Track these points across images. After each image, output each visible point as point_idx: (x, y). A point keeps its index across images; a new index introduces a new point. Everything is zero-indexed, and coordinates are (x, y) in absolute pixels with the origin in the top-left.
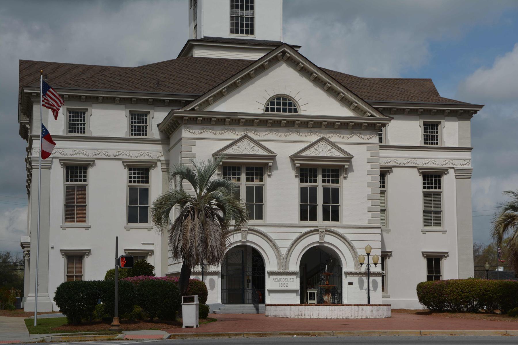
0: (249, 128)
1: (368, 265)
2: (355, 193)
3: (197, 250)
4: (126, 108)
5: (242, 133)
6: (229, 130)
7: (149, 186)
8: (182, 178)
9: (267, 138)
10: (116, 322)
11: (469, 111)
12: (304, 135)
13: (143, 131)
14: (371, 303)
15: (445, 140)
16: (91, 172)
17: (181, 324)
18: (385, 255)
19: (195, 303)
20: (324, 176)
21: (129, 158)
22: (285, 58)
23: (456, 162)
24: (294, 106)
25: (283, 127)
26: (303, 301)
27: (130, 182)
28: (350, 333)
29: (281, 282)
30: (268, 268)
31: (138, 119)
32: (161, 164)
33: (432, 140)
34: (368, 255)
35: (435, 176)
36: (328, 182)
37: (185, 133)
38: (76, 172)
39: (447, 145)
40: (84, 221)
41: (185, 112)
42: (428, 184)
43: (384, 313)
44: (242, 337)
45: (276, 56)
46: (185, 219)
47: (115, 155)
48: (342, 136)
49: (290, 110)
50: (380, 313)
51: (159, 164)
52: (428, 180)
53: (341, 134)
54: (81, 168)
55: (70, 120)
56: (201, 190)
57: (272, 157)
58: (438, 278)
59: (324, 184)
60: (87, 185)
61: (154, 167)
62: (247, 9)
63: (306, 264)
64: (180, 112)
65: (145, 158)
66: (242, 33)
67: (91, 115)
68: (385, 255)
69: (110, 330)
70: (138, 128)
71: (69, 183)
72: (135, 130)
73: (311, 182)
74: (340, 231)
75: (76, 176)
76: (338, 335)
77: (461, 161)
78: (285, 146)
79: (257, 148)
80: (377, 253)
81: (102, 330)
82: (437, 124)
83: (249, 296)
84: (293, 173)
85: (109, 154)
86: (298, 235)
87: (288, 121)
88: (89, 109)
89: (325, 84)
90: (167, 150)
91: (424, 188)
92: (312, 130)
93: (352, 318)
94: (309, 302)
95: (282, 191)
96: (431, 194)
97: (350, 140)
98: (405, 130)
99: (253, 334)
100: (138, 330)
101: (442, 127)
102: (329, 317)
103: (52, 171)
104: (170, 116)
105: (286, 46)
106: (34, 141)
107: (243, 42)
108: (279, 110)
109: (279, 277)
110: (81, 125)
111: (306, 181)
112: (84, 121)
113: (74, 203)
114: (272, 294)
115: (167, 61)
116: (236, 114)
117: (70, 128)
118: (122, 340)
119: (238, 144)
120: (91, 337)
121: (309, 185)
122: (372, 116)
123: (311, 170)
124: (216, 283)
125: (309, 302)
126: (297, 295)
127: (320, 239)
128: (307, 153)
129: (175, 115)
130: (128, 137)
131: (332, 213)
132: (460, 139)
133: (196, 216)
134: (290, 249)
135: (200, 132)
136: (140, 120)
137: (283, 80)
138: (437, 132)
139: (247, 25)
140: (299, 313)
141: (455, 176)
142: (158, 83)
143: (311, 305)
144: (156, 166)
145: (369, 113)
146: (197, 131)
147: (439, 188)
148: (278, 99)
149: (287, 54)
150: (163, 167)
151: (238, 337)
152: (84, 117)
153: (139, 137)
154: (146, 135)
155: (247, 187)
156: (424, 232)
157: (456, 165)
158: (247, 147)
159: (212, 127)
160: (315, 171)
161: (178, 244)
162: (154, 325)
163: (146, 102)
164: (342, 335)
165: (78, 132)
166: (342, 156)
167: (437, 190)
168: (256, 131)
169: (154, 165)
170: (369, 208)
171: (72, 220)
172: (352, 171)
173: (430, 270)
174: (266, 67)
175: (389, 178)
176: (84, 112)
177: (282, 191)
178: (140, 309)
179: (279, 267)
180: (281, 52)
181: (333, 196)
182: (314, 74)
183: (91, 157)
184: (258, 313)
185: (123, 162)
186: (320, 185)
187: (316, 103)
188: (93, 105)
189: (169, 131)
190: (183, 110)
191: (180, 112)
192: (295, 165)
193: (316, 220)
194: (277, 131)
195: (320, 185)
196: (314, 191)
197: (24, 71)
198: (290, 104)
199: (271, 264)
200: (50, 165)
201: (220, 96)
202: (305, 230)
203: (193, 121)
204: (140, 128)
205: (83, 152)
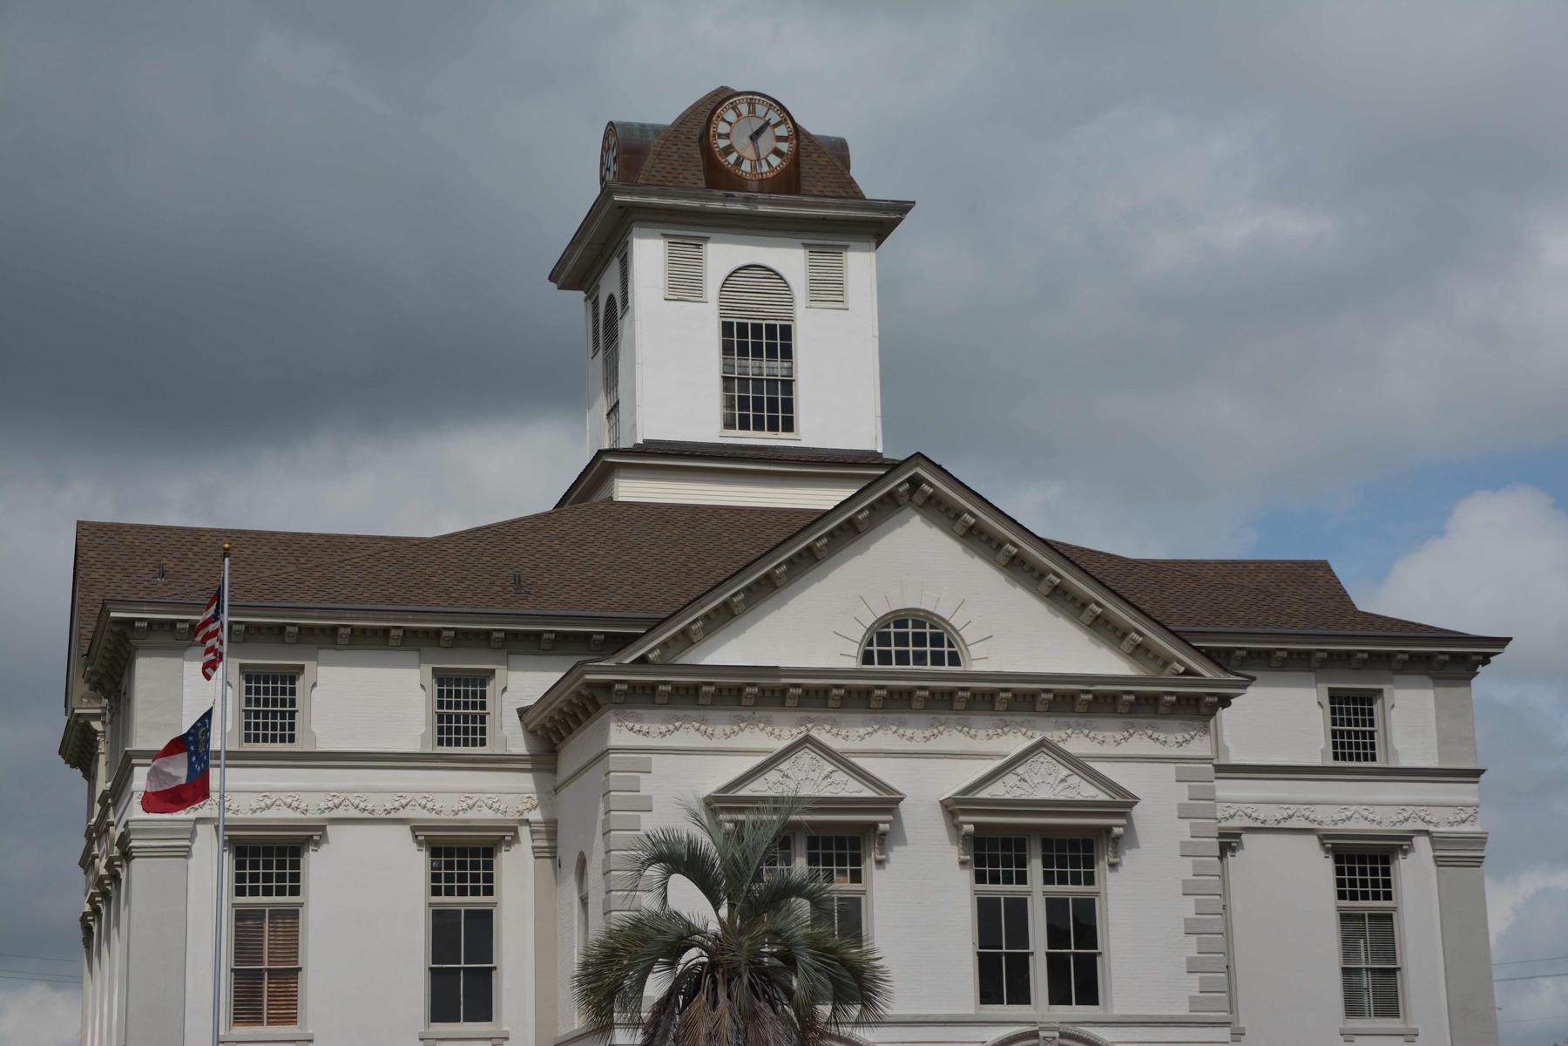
0: (813, 715)
2: (1141, 910)
4: (422, 661)
5: (794, 731)
6: (753, 722)
7: (495, 904)
8: (670, 873)
9: (868, 744)
11: (1465, 656)
12: (982, 733)
13: (474, 732)
15: (1397, 746)
16: (314, 864)
20: (1047, 862)
21: (433, 816)
22: (918, 499)
23: (1435, 815)
24: (950, 645)
25: (918, 711)
31: (458, 694)
32: (532, 832)
33: (457, 732)
35: (1373, 860)
36: (1063, 881)
37: (620, 733)
38: (268, 865)
39: (1405, 762)
40: (291, 1019)
41: (620, 668)
42: (1353, 883)
45: (890, 494)
46: (687, 1003)
47: (388, 806)
48: (1100, 736)
49: (938, 659)
51: (524, 832)
52: (1352, 871)
53: (1097, 728)
54: (281, 851)
55: (248, 701)
57: (889, 803)
59: (1050, 888)
60: (301, 905)
61: (510, 844)
62: (772, 354)
64: (603, 671)
65: (483, 815)
66: (759, 426)
67: (315, 685)
70: (459, 721)
72: (449, 729)
73: (1008, 881)
75: (267, 878)
77: (1439, 807)
78: (928, 771)
79: (841, 776)
85: (370, 807)
87: (933, 693)
88: (500, 671)
91: (1341, 896)
92: (1008, 719)
98: (1280, 717)
101: (1388, 706)
103: (191, 862)
104: (570, 679)
106: (136, 769)
107: (762, 454)
108: (902, 658)
110: (283, 717)
112: (293, 703)
113: (262, 963)
115: (537, 517)
116: (774, 671)
117: (247, 726)
119: (784, 766)
122: (1188, 672)
123: (1006, 844)
128: (996, 791)
129: (588, 677)
130: (429, 750)
131: (1078, 979)
132: (1443, 741)
133: (722, 994)
135: (663, 728)
137: (911, 565)
138: (1372, 724)
139: (773, 404)
141: (1435, 857)
142: (518, 581)
144: (515, 839)
145: (1181, 663)
146: (656, 728)
147: (1388, 896)
148: (901, 623)
150: (537, 844)
152: (293, 692)
153: (461, 750)
154: (483, 743)
155: (1048, 900)
157: (1437, 825)
158: (811, 775)
159: (701, 713)
160: (1021, 845)
163: (482, 639)
165: (274, 740)
168: (835, 723)
169: (508, 836)
171: (256, 1020)
172: (1134, 844)
176: (293, 674)
180: (908, 480)
181: (1077, 931)
182: (1009, 547)
183: (313, 815)
185: (414, 829)
188: (323, 654)
189: (556, 731)
190: (611, 663)
191: (603, 671)
192: (958, 827)
193: (1027, 1001)
194: (902, 724)
195: (1036, 891)
196: (1018, 908)
197: (92, 554)
198: (937, 640)
200: (187, 843)
201: (725, 616)
203: (643, 697)
204: (466, 721)
205: (289, 801)
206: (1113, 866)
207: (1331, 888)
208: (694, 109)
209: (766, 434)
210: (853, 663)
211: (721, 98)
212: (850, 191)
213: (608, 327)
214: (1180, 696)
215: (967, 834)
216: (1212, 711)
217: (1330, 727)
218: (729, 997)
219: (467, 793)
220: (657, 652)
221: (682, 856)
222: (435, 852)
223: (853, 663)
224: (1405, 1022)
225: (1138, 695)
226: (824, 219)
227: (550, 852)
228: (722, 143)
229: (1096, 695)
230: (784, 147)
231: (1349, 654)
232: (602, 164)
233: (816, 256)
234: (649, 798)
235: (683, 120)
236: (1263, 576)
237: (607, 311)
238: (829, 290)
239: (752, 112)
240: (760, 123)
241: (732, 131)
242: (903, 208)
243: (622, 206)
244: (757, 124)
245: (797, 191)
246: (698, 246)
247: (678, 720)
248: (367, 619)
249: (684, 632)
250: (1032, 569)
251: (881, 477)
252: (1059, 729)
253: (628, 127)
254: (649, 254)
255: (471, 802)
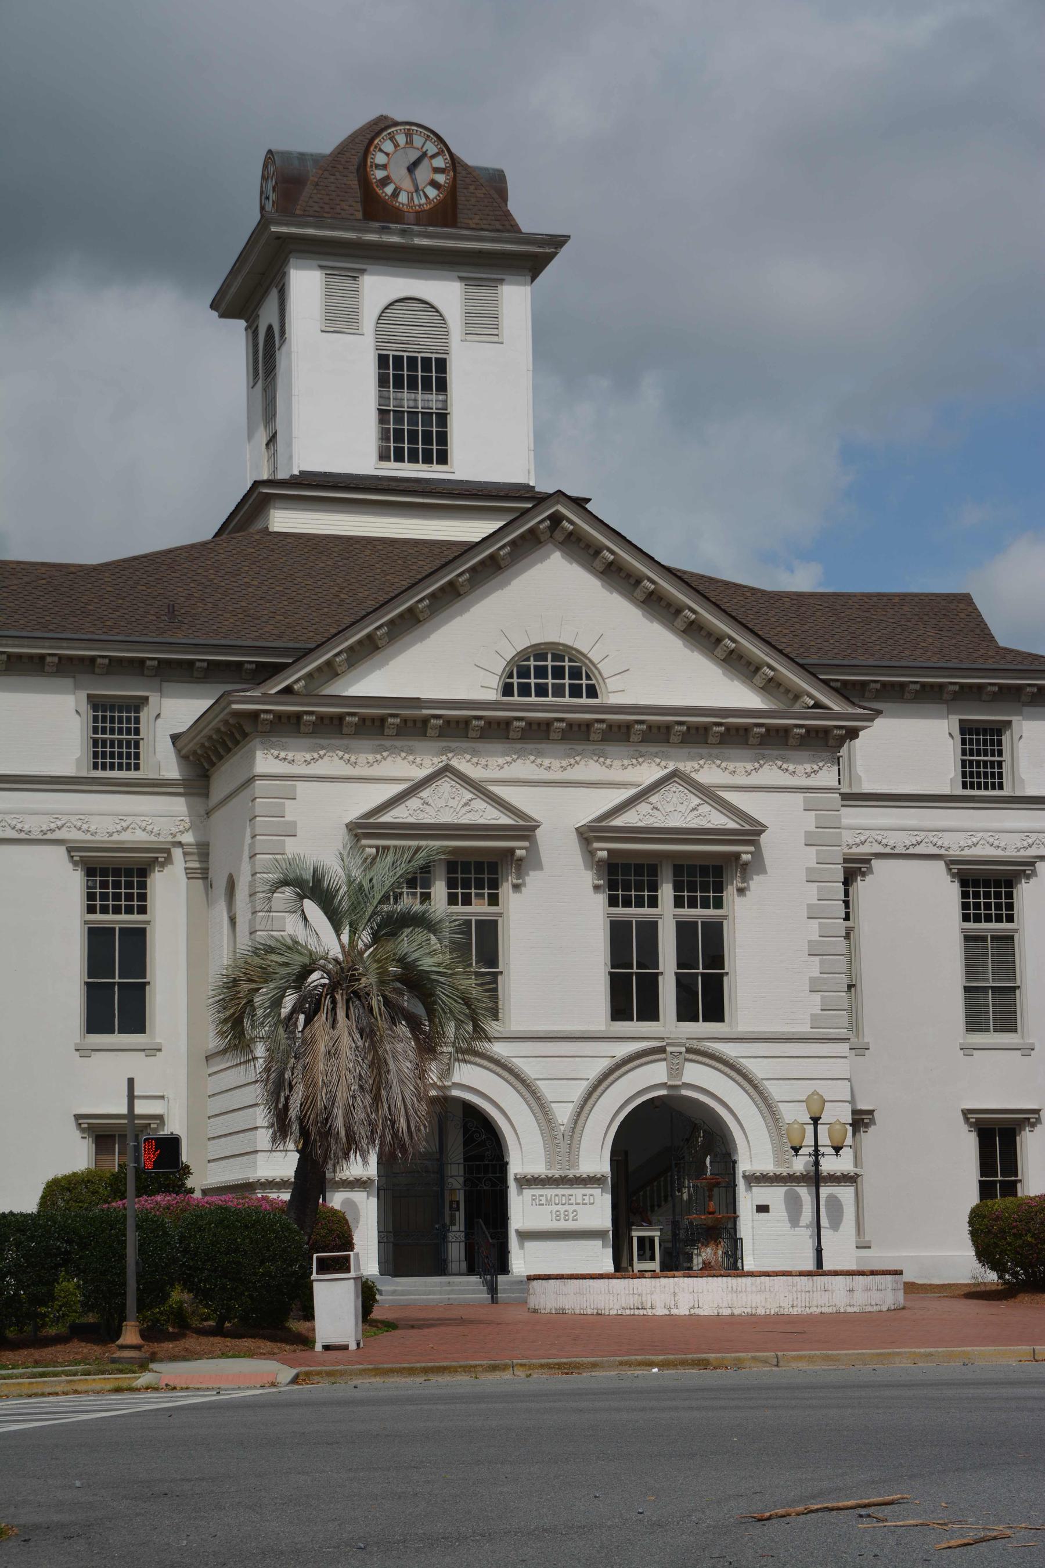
0: (453, 745)
1: (816, 1153)
2: (767, 931)
3: (349, 1111)
4: (77, 687)
5: (436, 760)
6: (394, 751)
8: (301, 897)
9: (508, 772)
10: (130, 1335)
12: (617, 763)
13: (129, 757)
14: (827, 1266)
15: (1023, 776)
16: (1026, 893)
17: (306, 1341)
18: (861, 1120)
19: (352, 1274)
20: (678, 887)
21: (88, 837)
22: (559, 536)
24: (588, 677)
26: (621, 1268)
27: (91, 910)
28: (827, 1358)
29: (555, 1208)
30: (517, 1166)
32: (185, 854)
34: (816, 1120)
35: (998, 884)
36: (692, 904)
37: (266, 761)
41: (266, 698)
43: (883, 1295)
44: (507, 1375)
45: (532, 531)
47: (45, 828)
48: (731, 766)
50: (876, 1297)
51: (177, 853)
52: (976, 895)
53: (728, 759)
56: (353, 932)
57: (526, 830)
58: (1010, 1188)
59: (680, 911)
61: (163, 865)
62: (427, 387)
63: (626, 1153)
64: (249, 700)
65: (137, 836)
66: (413, 458)
68: (861, 1120)
69: (114, 1361)
70: (114, 746)
71: (98, 917)
72: (104, 754)
73: (640, 904)
74: (729, 1050)
76: (794, 1365)
78: (563, 799)
79: (479, 804)
80: (839, 1114)
81: (76, 1363)
82: (997, 730)
83: (456, 1251)
84: (587, 878)
86: (604, 1064)
89: (678, 611)
90: (203, 812)
91: (966, 918)
92: (643, 749)
93: (795, 1311)
94: (638, 1266)
95: (554, 937)
96: (984, 939)
97: (755, 779)
98: (910, 747)
99: (542, 1366)
100: (185, 1359)
101: (1016, 737)
102: (726, 1312)
105: (562, 499)
107: (416, 487)
108: (542, 691)
109: (550, 1192)
111: (627, 903)
114: (528, 1245)
115: (193, 546)
118: (156, 1389)
119: (425, 794)
120: (60, 1382)
121: (634, 913)
122: (818, 705)
123: (639, 869)
124: (363, 1213)
125: (638, 1266)
126: (604, 1246)
127: (670, 1075)
128: (630, 819)
129: (235, 706)
130: (84, 774)
131: (704, 998)
133: (341, 1013)
134: (582, 1108)
135: (308, 757)
136: (120, 722)
137: (552, 600)
138: (1000, 754)
139: (427, 437)
140: (635, 1301)
142: (171, 611)
143: (642, 1274)
144: (169, 860)
146: (300, 756)
147: (143, 910)
148: (541, 656)
149: (565, 524)
151: (498, 1375)
153: (116, 774)
154: (137, 767)
155: (677, 923)
156: (967, 1050)
158: (451, 803)
159: (345, 742)
161: (287, 1098)
162: (229, 1342)
163: (136, 667)
164: (803, 1365)
166: (732, 825)
167: (1004, 925)
168: (475, 753)
170: (812, 980)
172: (762, 869)
173: (986, 1165)
174: (502, 564)
175: (862, 887)
177: (554, 937)
178: (187, 1297)
179: (550, 1165)
180: (549, 517)
182: (646, 583)
184: (494, 1300)
185: (69, 850)
186: (667, 913)
187: (651, 667)
189: (208, 756)
190: (257, 693)
191: (249, 700)
192: (592, 853)
193: (656, 1018)
194: (540, 754)
195: (667, 913)
196: (649, 930)
198: (576, 673)
199: (525, 1154)
201: (368, 650)
202: (624, 1049)
203: (287, 726)
206: (741, 891)
207: (956, 912)
208: (353, 139)
209: (420, 466)
210: (492, 695)
211: (381, 126)
212: (507, 224)
213: (266, 359)
214: (809, 730)
215: (600, 861)
216: (841, 741)
217: (959, 756)
218: (347, 1017)
219: (121, 816)
220: (302, 683)
221: (308, 882)
222: (90, 872)
223: (492, 695)
224: (1023, 1037)
225: (769, 729)
226: (480, 253)
227: (202, 874)
228: (380, 174)
229: (729, 728)
230: (441, 178)
231: (980, 687)
232: (262, 193)
233: (471, 289)
234: (294, 824)
235: (342, 149)
236: (906, 609)
237: (265, 345)
238: (484, 324)
239: (410, 142)
240: (418, 154)
241: (389, 161)
242: (558, 242)
243: (279, 237)
244: (414, 155)
245: (454, 224)
246: (355, 278)
247: (323, 748)
248: (23, 646)
249: (329, 663)
250: (669, 605)
251: (529, 510)
252: (692, 759)
253: (286, 155)
254: (306, 285)
255: (125, 824)
